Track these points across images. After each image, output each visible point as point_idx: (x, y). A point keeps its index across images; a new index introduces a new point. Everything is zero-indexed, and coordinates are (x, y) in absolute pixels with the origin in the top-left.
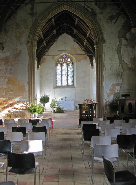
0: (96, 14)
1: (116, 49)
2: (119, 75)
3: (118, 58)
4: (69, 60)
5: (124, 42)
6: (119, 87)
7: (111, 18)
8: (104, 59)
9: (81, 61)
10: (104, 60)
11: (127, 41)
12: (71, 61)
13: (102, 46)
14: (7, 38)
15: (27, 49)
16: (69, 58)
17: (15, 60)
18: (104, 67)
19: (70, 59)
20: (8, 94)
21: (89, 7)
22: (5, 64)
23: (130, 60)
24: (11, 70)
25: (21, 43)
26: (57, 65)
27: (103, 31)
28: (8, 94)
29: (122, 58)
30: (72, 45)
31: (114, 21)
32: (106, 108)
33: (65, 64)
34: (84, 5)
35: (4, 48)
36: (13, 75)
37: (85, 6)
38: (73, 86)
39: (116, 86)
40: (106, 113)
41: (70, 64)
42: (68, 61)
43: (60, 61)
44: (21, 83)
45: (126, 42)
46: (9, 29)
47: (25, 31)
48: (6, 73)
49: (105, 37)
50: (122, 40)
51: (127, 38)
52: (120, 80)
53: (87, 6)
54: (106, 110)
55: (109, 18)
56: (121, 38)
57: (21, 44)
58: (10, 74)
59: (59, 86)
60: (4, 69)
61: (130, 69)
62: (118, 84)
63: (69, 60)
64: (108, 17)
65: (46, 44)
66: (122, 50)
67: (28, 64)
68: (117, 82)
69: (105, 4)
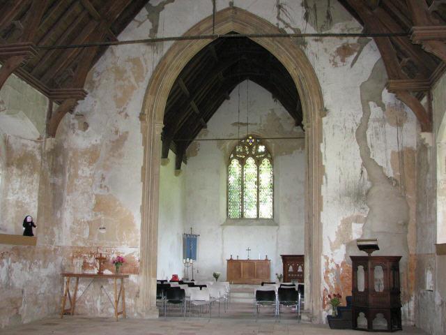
0: (307, 43)
1: (355, 131)
2: (359, 196)
3: (359, 154)
4: (262, 149)
5: (375, 111)
6: (361, 225)
7: (345, 51)
8: (323, 156)
9: (294, 152)
10: (323, 158)
11: (384, 109)
12: (267, 151)
13: (320, 123)
14: (95, 102)
15: (139, 131)
16: (262, 144)
17: (113, 156)
18: (324, 177)
19: (264, 147)
20: (96, 236)
21: (288, 25)
22: (90, 163)
23: (389, 157)
24: (103, 178)
25: (127, 115)
26: (229, 162)
27: (323, 86)
28: (96, 236)
29: (369, 153)
30: (270, 110)
31: (351, 58)
32: (326, 278)
33: (250, 161)
34: (276, 19)
35: (88, 126)
36: (108, 190)
37: (280, 22)
38: (272, 222)
39: (353, 224)
40: (326, 290)
41: (266, 161)
42: (259, 151)
43: (239, 153)
44: (124, 209)
45: (382, 111)
46: (99, 80)
47: (136, 85)
48: (91, 186)
49: (328, 100)
50: (369, 108)
51: (384, 101)
52: (363, 209)
53: (284, 22)
54: (327, 283)
55: (338, 51)
56: (368, 101)
57: (126, 118)
58: (101, 187)
59: (251, 219)
60: (88, 175)
61: (389, 180)
62: (357, 220)
63: (262, 149)
64: (335, 49)
65: (199, 107)
66: (369, 133)
67: (142, 164)
68: (356, 213)
69: (329, 16)
